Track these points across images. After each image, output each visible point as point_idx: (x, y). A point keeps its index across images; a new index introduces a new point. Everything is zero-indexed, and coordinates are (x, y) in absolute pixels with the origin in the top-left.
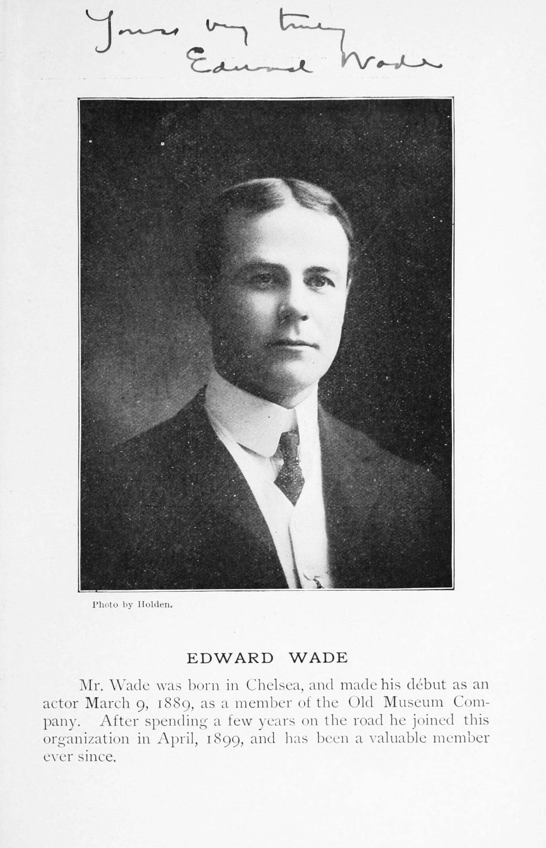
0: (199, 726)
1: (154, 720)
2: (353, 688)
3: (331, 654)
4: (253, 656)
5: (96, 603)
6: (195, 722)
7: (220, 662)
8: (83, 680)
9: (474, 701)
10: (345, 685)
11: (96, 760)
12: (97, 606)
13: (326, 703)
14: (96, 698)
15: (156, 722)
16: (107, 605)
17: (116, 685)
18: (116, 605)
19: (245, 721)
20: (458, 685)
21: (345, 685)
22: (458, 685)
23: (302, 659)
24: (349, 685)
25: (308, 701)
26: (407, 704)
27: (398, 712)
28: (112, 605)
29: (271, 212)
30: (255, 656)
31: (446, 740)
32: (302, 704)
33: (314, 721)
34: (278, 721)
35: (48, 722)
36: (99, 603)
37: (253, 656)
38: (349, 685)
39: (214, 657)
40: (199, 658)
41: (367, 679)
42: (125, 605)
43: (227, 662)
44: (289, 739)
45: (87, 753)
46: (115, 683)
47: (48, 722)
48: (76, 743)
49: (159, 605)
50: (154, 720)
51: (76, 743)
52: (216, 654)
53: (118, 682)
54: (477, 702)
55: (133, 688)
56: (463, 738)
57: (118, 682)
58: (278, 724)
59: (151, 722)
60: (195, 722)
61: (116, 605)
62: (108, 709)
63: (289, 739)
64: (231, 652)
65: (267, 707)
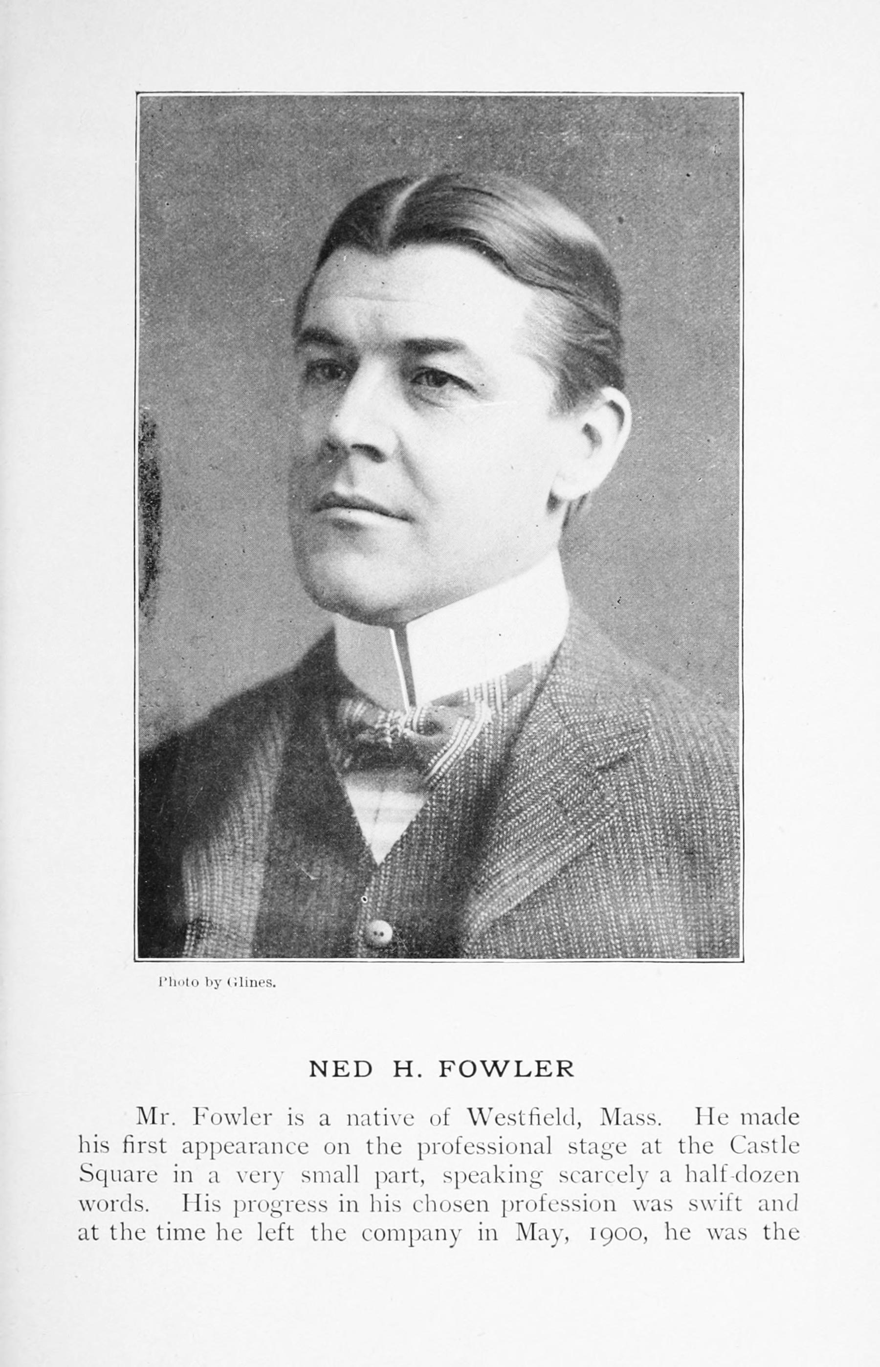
0: (270, 1211)
1: (457, 1173)
2: (359, 1123)
3: (473, 1063)
4: (564, 1065)
5: (163, 979)
6: (522, 1176)
7: (489, 1074)
8: (142, 1108)
9: (340, 1144)
10: (747, 1118)
11: (190, 1239)
12: (166, 984)
13: (694, 1147)
14: (153, 1108)
15: (461, 1177)
16: (181, 983)
17: (612, 1117)
18: (195, 983)
19: (706, 1203)
20: (770, 1118)
21: (747, 1118)
22: (770, 1118)
23: (501, 1070)
24: (754, 1118)
25: (458, 1143)
26: (312, 1176)
27: (338, 1163)
28: (190, 983)
29: (345, 404)
30: (568, 1065)
31: (334, 1236)
32: (436, 1120)
33: (344, 1147)
34: (485, 1175)
35: (382, 1177)
36: (168, 980)
37: (564, 1065)
38: (754, 1118)
39: (480, 1066)
40: (351, 1068)
41: (784, 1108)
42: (209, 983)
43: (500, 1074)
44: (692, 1175)
45: (169, 1226)
46: (713, 1232)
47: (382, 1177)
48: (349, 1210)
49: (242, 982)
50: (457, 1173)
51: (349, 1210)
52: (483, 1062)
53: (481, 1112)
54: (393, 1234)
55: (773, 1120)
56: (400, 1234)
57: (481, 1112)
58: (241, 1150)
59: (453, 1176)
60: (522, 1176)
61: (195, 983)
62: (546, 1155)
63: (692, 1175)
64: (483, 1059)
65: (348, 1153)
